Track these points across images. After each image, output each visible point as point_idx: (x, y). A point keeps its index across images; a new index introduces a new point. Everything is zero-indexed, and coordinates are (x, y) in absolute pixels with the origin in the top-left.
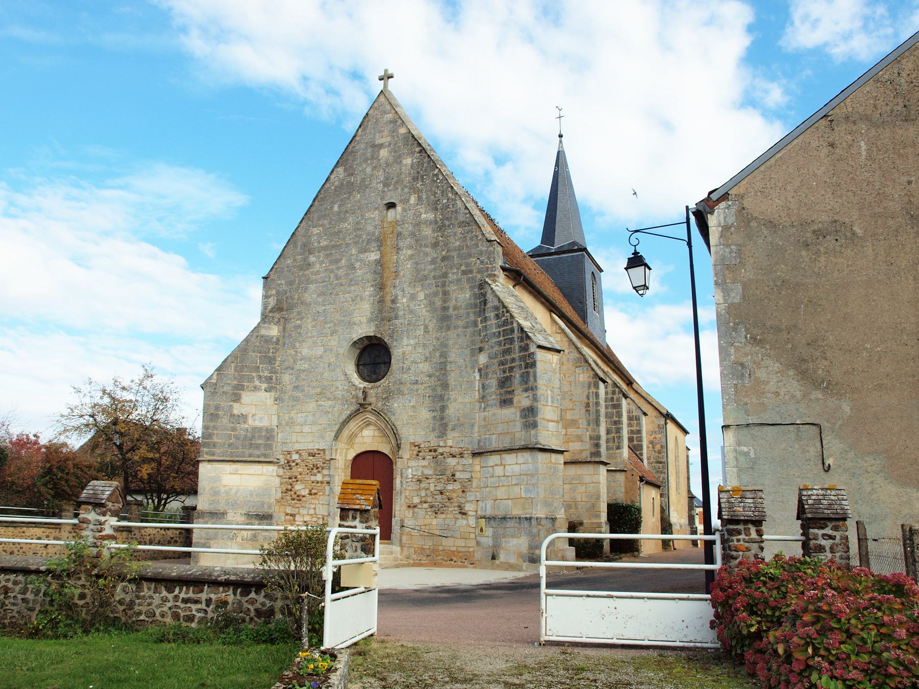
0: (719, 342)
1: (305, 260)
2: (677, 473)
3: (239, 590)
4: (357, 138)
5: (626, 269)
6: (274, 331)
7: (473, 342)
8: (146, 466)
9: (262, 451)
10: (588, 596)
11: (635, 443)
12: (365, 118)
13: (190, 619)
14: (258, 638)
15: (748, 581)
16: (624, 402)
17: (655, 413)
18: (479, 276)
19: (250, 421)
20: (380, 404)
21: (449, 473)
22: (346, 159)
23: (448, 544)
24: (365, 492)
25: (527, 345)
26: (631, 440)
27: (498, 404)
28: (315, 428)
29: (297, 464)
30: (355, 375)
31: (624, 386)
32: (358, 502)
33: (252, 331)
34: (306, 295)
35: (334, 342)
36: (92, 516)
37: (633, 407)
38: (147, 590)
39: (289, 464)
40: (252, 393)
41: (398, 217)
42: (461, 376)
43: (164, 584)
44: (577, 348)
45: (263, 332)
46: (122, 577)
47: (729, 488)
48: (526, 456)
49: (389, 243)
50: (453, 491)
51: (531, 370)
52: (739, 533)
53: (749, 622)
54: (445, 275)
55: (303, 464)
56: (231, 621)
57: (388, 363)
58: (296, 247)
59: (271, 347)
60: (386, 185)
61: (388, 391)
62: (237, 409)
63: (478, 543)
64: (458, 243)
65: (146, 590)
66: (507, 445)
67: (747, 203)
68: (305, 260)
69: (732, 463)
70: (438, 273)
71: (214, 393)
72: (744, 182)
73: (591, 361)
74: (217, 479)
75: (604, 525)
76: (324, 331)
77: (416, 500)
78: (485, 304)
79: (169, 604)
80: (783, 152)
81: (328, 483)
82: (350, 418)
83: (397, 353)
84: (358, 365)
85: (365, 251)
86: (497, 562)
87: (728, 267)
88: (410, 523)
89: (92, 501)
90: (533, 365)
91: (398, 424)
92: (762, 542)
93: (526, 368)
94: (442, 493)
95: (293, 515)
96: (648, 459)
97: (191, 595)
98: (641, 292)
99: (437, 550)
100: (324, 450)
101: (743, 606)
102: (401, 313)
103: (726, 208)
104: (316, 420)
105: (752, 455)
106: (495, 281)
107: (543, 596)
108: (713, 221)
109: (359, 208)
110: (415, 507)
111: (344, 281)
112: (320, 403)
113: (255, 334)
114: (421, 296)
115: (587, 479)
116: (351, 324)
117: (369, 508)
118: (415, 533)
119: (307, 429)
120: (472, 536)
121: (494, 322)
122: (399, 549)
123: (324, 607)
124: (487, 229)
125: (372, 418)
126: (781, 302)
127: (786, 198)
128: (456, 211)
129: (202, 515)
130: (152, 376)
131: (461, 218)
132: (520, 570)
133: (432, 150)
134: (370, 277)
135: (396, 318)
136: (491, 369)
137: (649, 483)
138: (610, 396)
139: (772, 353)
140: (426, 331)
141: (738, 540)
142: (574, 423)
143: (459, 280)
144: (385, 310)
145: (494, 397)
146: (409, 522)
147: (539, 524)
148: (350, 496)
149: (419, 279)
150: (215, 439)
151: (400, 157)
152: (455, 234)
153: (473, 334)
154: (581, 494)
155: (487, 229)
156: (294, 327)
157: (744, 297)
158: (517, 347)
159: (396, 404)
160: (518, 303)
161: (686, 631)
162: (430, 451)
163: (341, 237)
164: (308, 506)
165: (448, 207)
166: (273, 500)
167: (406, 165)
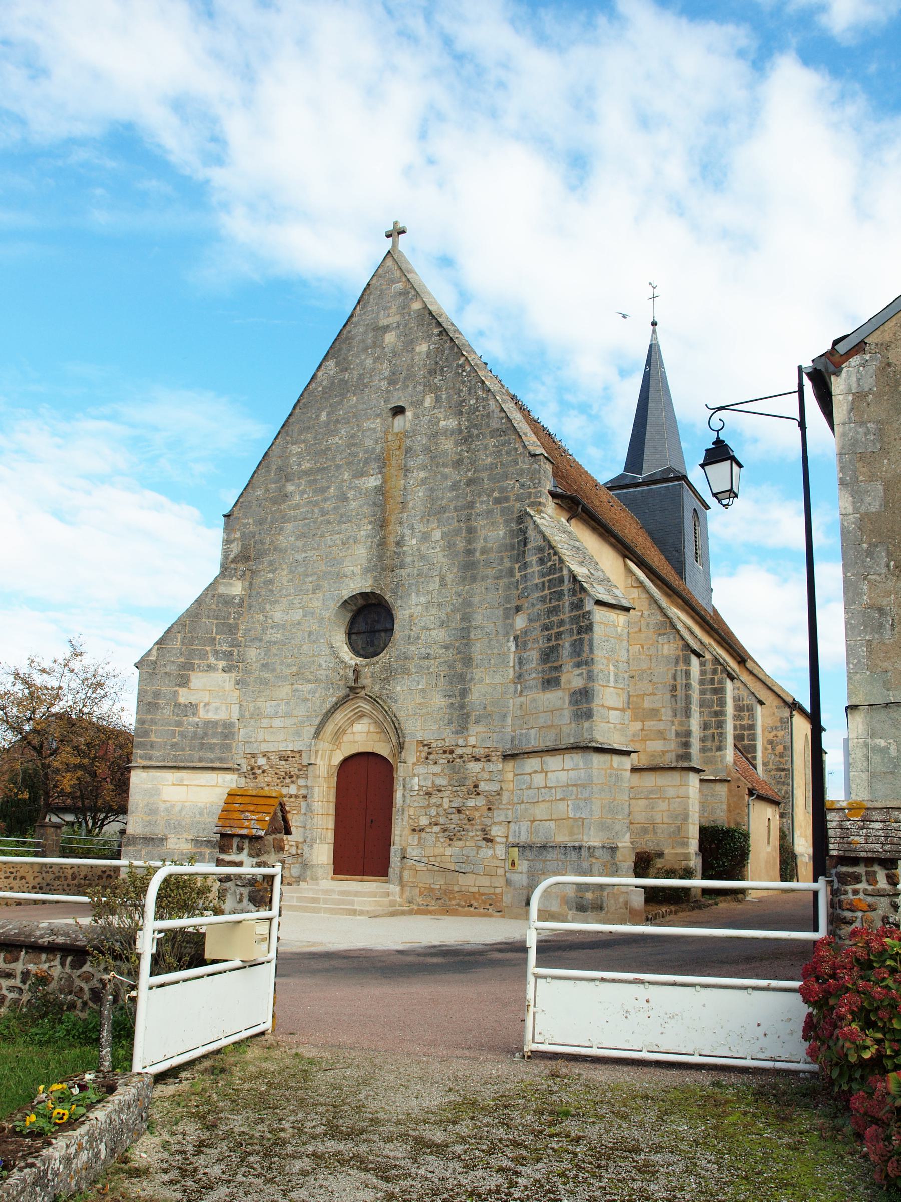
0: (845, 574)
3: (69, 959)
4: (355, 319)
6: (237, 589)
7: (507, 599)
9: (217, 753)
11: (746, 742)
12: (365, 290)
15: (867, 965)
16: (729, 685)
17: (777, 702)
19: (202, 713)
20: (377, 688)
21: (469, 783)
22: (337, 349)
23: (467, 883)
24: (260, 809)
25: (581, 600)
26: (738, 738)
28: (289, 722)
30: (346, 648)
31: (732, 664)
32: (246, 823)
33: (207, 589)
34: (281, 538)
37: (744, 693)
40: (204, 674)
41: (408, 425)
42: (490, 647)
44: (661, 608)
45: (222, 590)
48: (574, 760)
49: (394, 462)
50: (475, 808)
52: (857, 879)
53: (860, 1042)
54: (471, 505)
55: (272, 771)
58: (269, 472)
59: (232, 610)
60: (392, 382)
62: (184, 696)
63: (508, 883)
66: (550, 744)
68: (281, 489)
69: (861, 764)
70: (461, 502)
71: (153, 674)
72: (891, 324)
73: (680, 626)
74: (156, 792)
75: (693, 857)
76: (304, 587)
77: (424, 821)
78: (525, 545)
82: (336, 707)
83: (401, 615)
84: (349, 634)
87: (862, 457)
88: (415, 853)
90: (589, 628)
91: (401, 715)
92: (897, 895)
93: (579, 633)
94: (459, 812)
96: (765, 764)
98: (725, 502)
99: (451, 892)
100: (300, 752)
101: (852, 1013)
102: (409, 560)
103: (860, 365)
105: (893, 752)
106: (540, 512)
107: (531, 979)
108: (838, 386)
109: (355, 416)
110: (422, 830)
111: (332, 518)
112: (296, 686)
113: (210, 593)
114: (437, 535)
115: (671, 792)
116: (340, 577)
117: (262, 833)
118: (420, 867)
119: (277, 723)
120: (500, 872)
122: (398, 889)
123: (134, 1000)
124: (531, 439)
128: (488, 415)
129: (133, 840)
131: (495, 424)
133: (456, 330)
134: (367, 510)
135: (402, 567)
137: (761, 798)
138: (709, 676)
140: (443, 583)
141: (856, 892)
142: (654, 713)
143: (489, 512)
144: (387, 557)
146: (413, 852)
147: (591, 856)
148: (236, 815)
149: (435, 511)
150: (153, 738)
151: (412, 342)
152: (486, 447)
153: (508, 588)
154: (661, 813)
155: (531, 439)
156: (265, 582)
157: (886, 503)
158: (567, 604)
159: (399, 688)
160: (572, 543)
161: (764, 1042)
162: (445, 752)
165: (476, 409)
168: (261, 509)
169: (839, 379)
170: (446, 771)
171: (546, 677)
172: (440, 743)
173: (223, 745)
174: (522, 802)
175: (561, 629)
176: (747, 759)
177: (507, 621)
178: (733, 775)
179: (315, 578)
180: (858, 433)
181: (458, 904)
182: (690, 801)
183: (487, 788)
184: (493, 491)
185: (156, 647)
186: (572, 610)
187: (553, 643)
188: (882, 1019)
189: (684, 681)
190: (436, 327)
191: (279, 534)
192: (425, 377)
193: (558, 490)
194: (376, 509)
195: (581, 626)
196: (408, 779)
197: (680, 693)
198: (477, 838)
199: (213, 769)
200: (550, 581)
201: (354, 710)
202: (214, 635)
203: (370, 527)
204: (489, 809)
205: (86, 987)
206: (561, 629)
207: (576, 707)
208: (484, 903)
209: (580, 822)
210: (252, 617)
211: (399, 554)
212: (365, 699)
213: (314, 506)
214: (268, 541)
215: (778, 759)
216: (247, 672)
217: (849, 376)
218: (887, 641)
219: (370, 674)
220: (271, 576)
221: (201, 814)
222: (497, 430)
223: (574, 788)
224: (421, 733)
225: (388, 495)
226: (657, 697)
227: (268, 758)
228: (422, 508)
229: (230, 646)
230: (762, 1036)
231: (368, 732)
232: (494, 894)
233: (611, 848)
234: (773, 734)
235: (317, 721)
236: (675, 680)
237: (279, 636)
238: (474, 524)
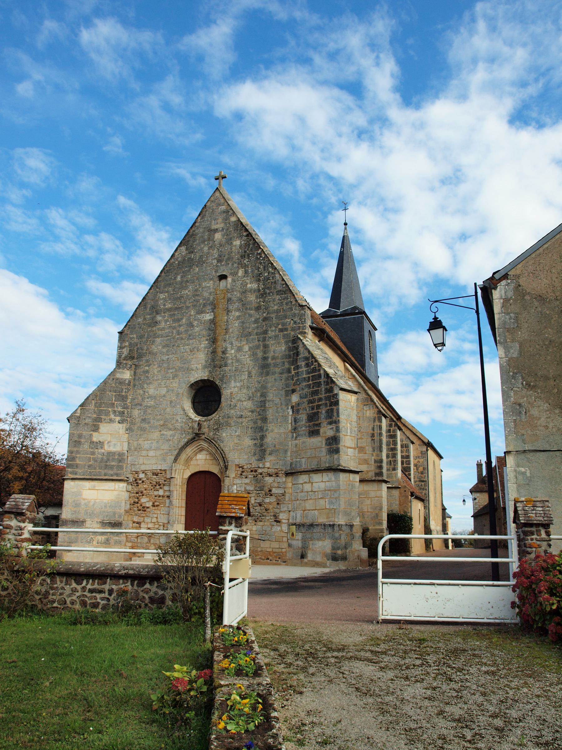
0: (502, 387)
1: (153, 319)
2: (435, 489)
3: (136, 582)
4: (197, 224)
5: (429, 330)
6: (127, 375)
7: (287, 385)
8: (17, 483)
9: (115, 471)
10: (415, 584)
12: (203, 208)
13: (95, 605)
14: (155, 621)
15: (546, 570)
16: (399, 433)
18: (293, 333)
20: (211, 434)
21: (266, 489)
24: (239, 503)
25: (332, 388)
27: (307, 434)
28: (159, 453)
29: (143, 482)
30: (192, 411)
32: (234, 511)
33: (109, 375)
34: (153, 347)
35: (175, 384)
36: (14, 523)
37: (404, 438)
38: (59, 583)
39: (136, 482)
40: (108, 424)
41: (229, 286)
42: (277, 412)
43: (74, 577)
45: (118, 376)
46: (41, 573)
47: (523, 499)
48: (327, 476)
49: (221, 306)
50: (270, 503)
51: (335, 408)
52: (532, 534)
54: (265, 332)
56: (131, 608)
57: (219, 402)
58: (146, 308)
60: (219, 261)
61: (218, 423)
62: (96, 437)
63: (290, 546)
64: (276, 307)
65: (58, 583)
66: (314, 467)
67: (522, 281)
68: (153, 319)
72: (520, 266)
74: (79, 494)
76: (167, 375)
78: (298, 355)
79: (78, 594)
80: (549, 243)
81: (168, 497)
83: (226, 393)
85: (202, 312)
86: (305, 560)
89: (14, 510)
90: (337, 403)
91: (226, 450)
93: (330, 406)
94: (260, 505)
95: (139, 523)
97: (96, 586)
99: (257, 551)
100: (165, 470)
102: (229, 362)
103: (506, 285)
104: (160, 447)
105: (528, 475)
106: (305, 337)
107: (380, 584)
108: (497, 295)
109: (197, 279)
111: (184, 336)
112: (162, 432)
113: (112, 377)
114: (246, 348)
115: (372, 494)
116: (189, 370)
117: (243, 515)
119: (151, 453)
120: (285, 539)
121: (304, 369)
123: (223, 594)
125: (205, 445)
126: (549, 357)
127: (551, 278)
128: (275, 283)
130: (23, 410)
131: (279, 287)
132: (324, 567)
134: (205, 333)
135: (226, 365)
136: (301, 407)
137: (417, 498)
139: (542, 396)
140: (250, 375)
141: (532, 539)
143: (276, 336)
144: (216, 359)
145: (304, 428)
147: (340, 530)
148: (227, 506)
150: (78, 462)
151: (231, 239)
152: (274, 300)
153: (287, 379)
154: (367, 506)
156: (143, 372)
157: (520, 353)
158: (323, 389)
159: (224, 434)
160: (324, 355)
161: (492, 610)
162: (252, 471)
163: (183, 301)
164: (151, 515)
165: (268, 279)
166: (122, 511)
167: (235, 246)
168: (141, 330)
169: (496, 292)
170: (253, 482)
171: (311, 429)
172: (249, 466)
173: (118, 466)
174: (298, 500)
175: (320, 403)
176: (406, 475)
177: (287, 398)
178: (402, 484)
179: (174, 370)
180: (506, 318)
181: (261, 558)
182: (383, 499)
183: (276, 492)
184: (279, 325)
185: (80, 408)
186: (326, 393)
187: (315, 411)
188: (558, 592)
189: (379, 432)
190: (245, 232)
191: (152, 344)
192: (238, 259)
193: (314, 325)
194: (210, 332)
195: (332, 402)
196: (230, 487)
197: (376, 438)
198: (271, 520)
199: (113, 480)
200: (312, 376)
201: (197, 446)
202: (113, 402)
203: (207, 342)
204: (278, 504)
205: (147, 597)
206: (320, 403)
207: (329, 447)
208: (276, 557)
209: (333, 512)
210: (136, 392)
211: (224, 358)
212: (204, 440)
213: (174, 329)
214: (145, 348)
215: (420, 475)
216: (132, 423)
217: (501, 290)
218: (523, 420)
219: (207, 426)
220: (147, 368)
221: (105, 507)
222: (281, 291)
223: (329, 492)
224: (238, 460)
225: (217, 324)
226: (363, 440)
227: (146, 474)
228: (237, 333)
229: (123, 408)
230: (490, 608)
231: (206, 460)
232: (282, 552)
233: (350, 525)
234: (417, 460)
235: (176, 453)
236: (374, 431)
237: (152, 403)
238: (267, 343)
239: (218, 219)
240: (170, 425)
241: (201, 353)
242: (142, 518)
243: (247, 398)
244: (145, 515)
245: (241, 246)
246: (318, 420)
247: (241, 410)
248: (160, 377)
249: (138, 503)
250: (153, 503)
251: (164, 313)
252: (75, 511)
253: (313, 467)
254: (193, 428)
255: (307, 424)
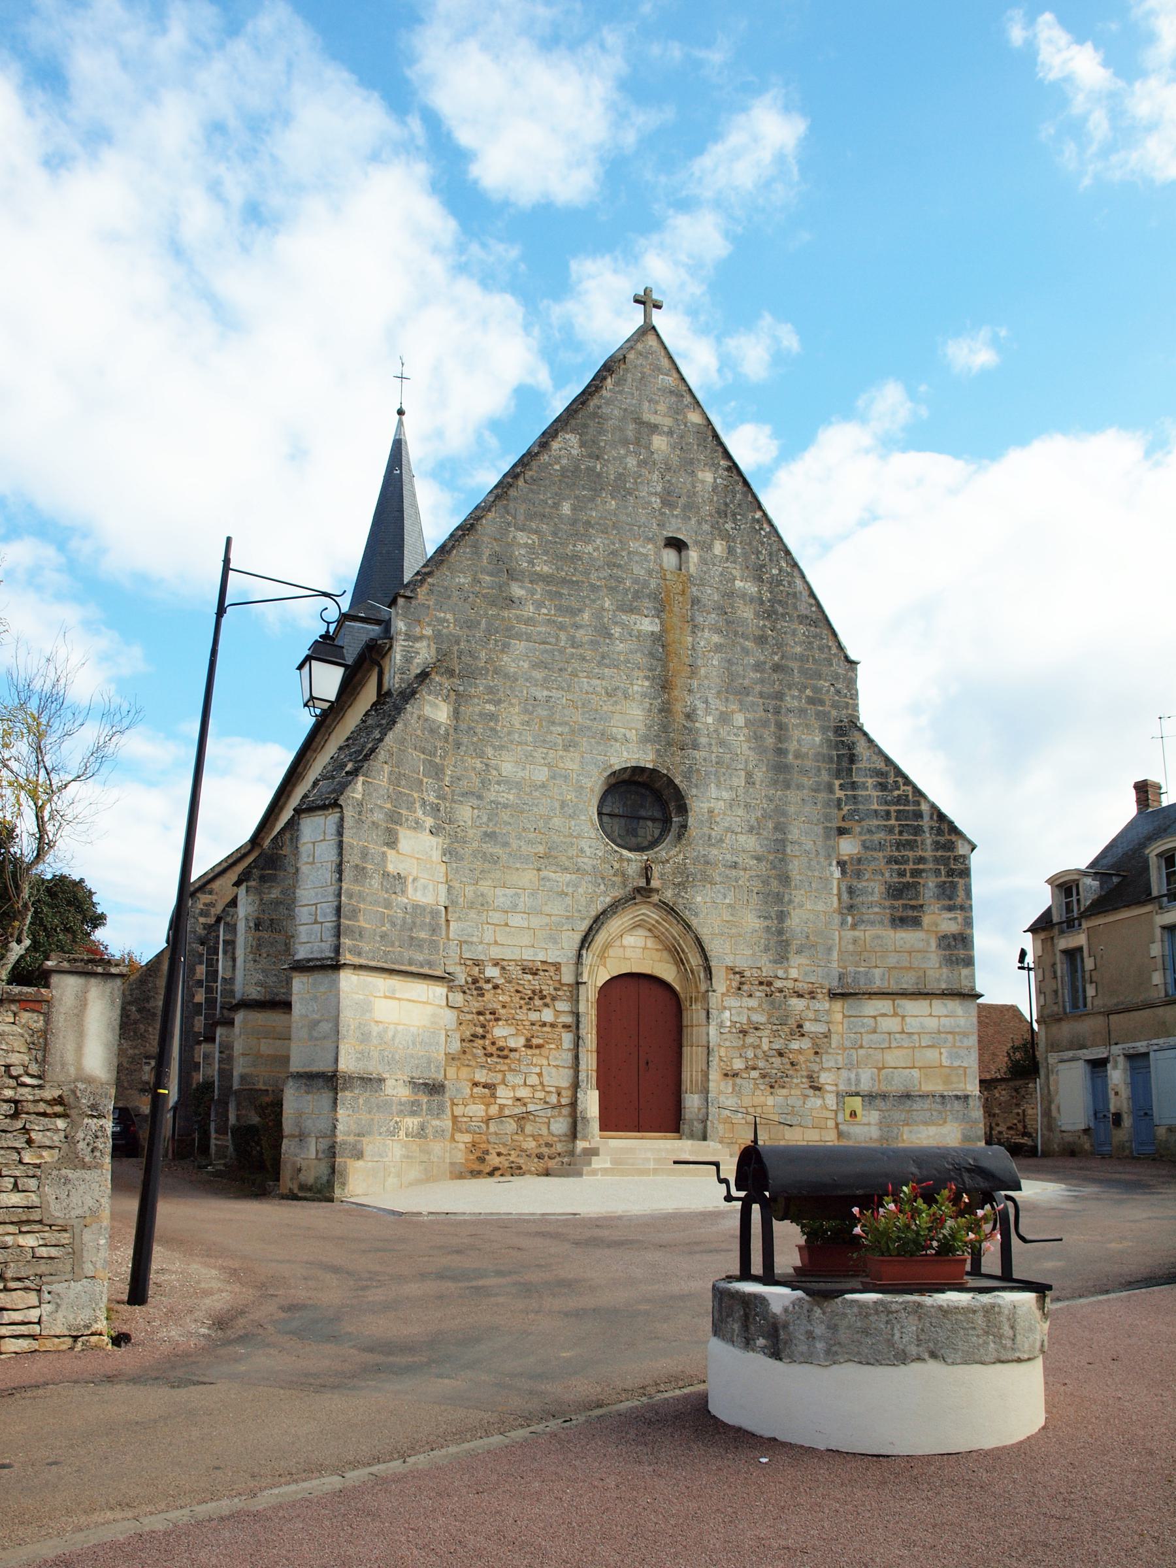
7: (828, 818)
21: (792, 1022)
27: (886, 922)
29: (496, 987)
39: (476, 985)
42: (809, 868)
51: (961, 882)
54: (779, 696)
58: (477, 552)
76: (549, 738)
94: (781, 1055)
102: (703, 740)
109: (614, 526)
112: (544, 873)
114: (739, 719)
119: (516, 920)
120: (831, 1124)
125: (654, 915)
131: (803, 609)
135: (695, 746)
140: (750, 781)
144: (670, 724)
156: (481, 714)
158: (929, 841)
162: (761, 983)
165: (780, 583)
170: (764, 1006)
174: (861, 1047)
175: (921, 866)
179: (567, 730)
183: (813, 1029)
184: (806, 688)
187: (908, 879)
191: (502, 651)
194: (655, 663)
202: (421, 776)
204: (816, 1053)
206: (921, 866)
220: (490, 708)
223: (950, 1037)
227: (503, 968)
231: (645, 948)
235: (584, 926)
237: (511, 797)
239: (657, 402)
240: (564, 858)
241: (634, 705)
242: (500, 1076)
243: (747, 828)
244: (506, 1068)
245: (715, 488)
246: (916, 898)
247: (734, 852)
248: (530, 739)
249: (484, 1037)
250: (528, 1040)
251: (531, 582)
252: (361, 1053)
253: (905, 986)
254: (624, 875)
255: (887, 903)
